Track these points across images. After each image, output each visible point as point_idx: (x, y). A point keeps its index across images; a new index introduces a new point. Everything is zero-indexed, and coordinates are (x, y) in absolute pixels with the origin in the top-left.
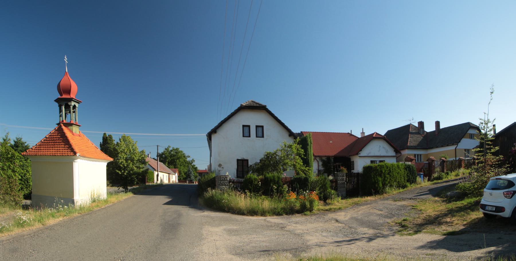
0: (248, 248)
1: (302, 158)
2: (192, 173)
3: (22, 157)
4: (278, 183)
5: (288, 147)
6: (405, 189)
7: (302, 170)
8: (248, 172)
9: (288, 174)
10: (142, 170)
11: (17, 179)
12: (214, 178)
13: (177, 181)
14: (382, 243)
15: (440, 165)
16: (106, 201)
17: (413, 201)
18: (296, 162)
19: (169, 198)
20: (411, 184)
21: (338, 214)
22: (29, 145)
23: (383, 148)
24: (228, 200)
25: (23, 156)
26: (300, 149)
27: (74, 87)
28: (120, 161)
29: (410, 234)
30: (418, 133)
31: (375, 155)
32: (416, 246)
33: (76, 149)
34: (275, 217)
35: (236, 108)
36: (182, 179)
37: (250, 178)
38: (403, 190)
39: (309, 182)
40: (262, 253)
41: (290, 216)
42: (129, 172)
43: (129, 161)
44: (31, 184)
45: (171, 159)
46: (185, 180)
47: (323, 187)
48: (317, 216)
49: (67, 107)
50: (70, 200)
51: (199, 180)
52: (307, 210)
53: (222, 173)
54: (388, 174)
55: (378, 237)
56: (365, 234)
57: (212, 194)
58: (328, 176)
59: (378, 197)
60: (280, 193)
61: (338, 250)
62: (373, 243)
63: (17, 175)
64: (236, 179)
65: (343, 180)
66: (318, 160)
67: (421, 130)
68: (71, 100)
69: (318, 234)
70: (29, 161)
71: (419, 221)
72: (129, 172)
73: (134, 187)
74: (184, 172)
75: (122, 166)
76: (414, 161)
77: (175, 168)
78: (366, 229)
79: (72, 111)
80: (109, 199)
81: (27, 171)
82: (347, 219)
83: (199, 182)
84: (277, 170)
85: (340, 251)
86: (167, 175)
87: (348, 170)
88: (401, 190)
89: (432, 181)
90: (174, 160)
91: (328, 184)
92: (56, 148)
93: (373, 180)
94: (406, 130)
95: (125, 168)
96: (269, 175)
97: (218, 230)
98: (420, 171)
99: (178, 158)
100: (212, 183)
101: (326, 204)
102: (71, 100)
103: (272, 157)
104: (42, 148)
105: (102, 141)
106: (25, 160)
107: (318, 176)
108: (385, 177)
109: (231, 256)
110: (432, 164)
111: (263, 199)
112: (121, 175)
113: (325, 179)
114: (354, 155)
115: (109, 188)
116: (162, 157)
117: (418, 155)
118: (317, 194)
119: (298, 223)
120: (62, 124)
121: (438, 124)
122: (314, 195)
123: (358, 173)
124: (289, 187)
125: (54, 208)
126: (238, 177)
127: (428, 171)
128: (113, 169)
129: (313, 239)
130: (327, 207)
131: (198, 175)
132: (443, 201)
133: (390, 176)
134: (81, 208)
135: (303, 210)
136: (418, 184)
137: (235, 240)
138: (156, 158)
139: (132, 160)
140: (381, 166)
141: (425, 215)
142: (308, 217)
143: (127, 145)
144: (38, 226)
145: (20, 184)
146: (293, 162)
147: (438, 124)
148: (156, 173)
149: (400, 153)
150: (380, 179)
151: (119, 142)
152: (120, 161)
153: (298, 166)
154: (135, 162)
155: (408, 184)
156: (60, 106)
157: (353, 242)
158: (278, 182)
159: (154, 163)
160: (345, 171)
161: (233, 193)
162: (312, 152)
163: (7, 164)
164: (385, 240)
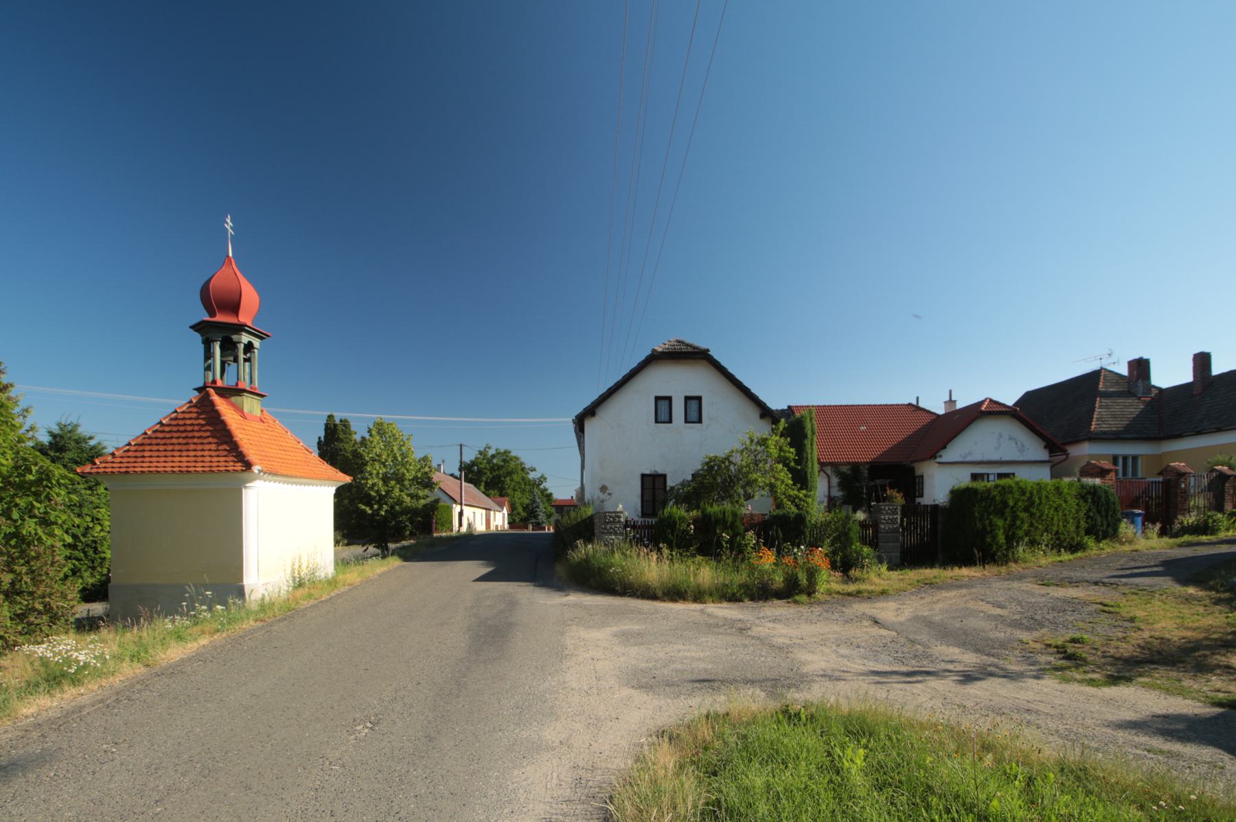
0: (666, 672)
1: (791, 470)
2: (541, 506)
3: (77, 478)
4: (733, 526)
5: (758, 443)
6: (1079, 554)
7: (789, 497)
8: (664, 504)
9: (757, 505)
10: (422, 502)
11: (59, 544)
12: (591, 518)
13: (506, 526)
14: (1003, 692)
15: (1210, 487)
16: (332, 582)
17: (1103, 589)
18: (777, 479)
19: (488, 566)
20: (1098, 540)
21: (879, 605)
22: (105, 444)
23: (1011, 438)
24: (622, 567)
25: (83, 475)
26: (786, 449)
27: (250, 297)
28: (370, 482)
29: (1091, 682)
30: (1129, 394)
31: (987, 458)
32: (1110, 718)
33: (251, 455)
34: (725, 604)
35: (642, 357)
36: (517, 520)
37: (670, 516)
38: (1071, 557)
39: (805, 526)
40: (697, 685)
41: (761, 603)
42: (392, 507)
43: (393, 483)
44: (108, 555)
45: (491, 476)
46: (524, 523)
47: (842, 539)
48: (826, 607)
49: (229, 347)
50: (230, 586)
51: (557, 522)
52: (801, 592)
53: (608, 507)
54: (1026, 510)
55: (992, 675)
56: (951, 662)
57: (587, 555)
58: (855, 511)
59: (990, 570)
60: (738, 550)
61: (881, 693)
62: (978, 690)
63: (58, 532)
64: (640, 520)
65: (894, 521)
66: (829, 472)
67: (1140, 383)
68: (240, 328)
69: (827, 651)
70: (101, 490)
71: (1126, 650)
72: (392, 507)
73: (405, 543)
74: (521, 504)
75: (373, 494)
76: (1112, 475)
77: (501, 495)
78: (957, 650)
79: (242, 356)
80: (341, 577)
81: (95, 520)
82: (902, 619)
83: (556, 527)
84: (731, 496)
85: (884, 695)
86: (484, 512)
87: (906, 496)
88: (1066, 556)
89: (1176, 536)
90: (499, 477)
91: (855, 531)
92: (192, 453)
93: (979, 525)
94: (1086, 387)
95: (381, 500)
96: (714, 509)
97: (601, 635)
98: (1134, 505)
99: (510, 473)
100: (587, 529)
101: (848, 579)
102: (240, 328)
103: (719, 467)
104: (147, 454)
105: (322, 434)
106: (90, 488)
107: (829, 511)
108: (1015, 518)
109: (627, 691)
110: (1177, 484)
111: (699, 564)
112: (372, 515)
113: (848, 518)
114: (923, 460)
115: (340, 548)
116: (472, 472)
117: (1125, 458)
118: (826, 555)
119: (780, 621)
120: (211, 391)
121: (1202, 361)
122: (819, 558)
123: (935, 507)
124: (759, 537)
125: (182, 615)
126: (644, 514)
127: (1162, 505)
128: (352, 501)
129: (815, 661)
130: (852, 588)
131: (553, 510)
132: (1218, 602)
133: (1032, 515)
134: (264, 606)
135: (791, 590)
136: (1122, 543)
137: (636, 655)
138: (457, 473)
139: (400, 479)
140: (1003, 487)
141: (1146, 635)
142: (802, 609)
143: (388, 445)
144: (130, 670)
145: (68, 558)
146: (768, 479)
147: (1202, 361)
148: (456, 509)
149: (1065, 452)
150: (1000, 523)
151: (367, 436)
152: (370, 482)
153: (781, 488)
154: (407, 483)
155: (1090, 541)
156: (208, 344)
157: (920, 678)
158: (734, 525)
159: (451, 486)
160: (899, 499)
161: (633, 552)
162: (816, 453)
163: (22, 502)
164: (1011, 685)
